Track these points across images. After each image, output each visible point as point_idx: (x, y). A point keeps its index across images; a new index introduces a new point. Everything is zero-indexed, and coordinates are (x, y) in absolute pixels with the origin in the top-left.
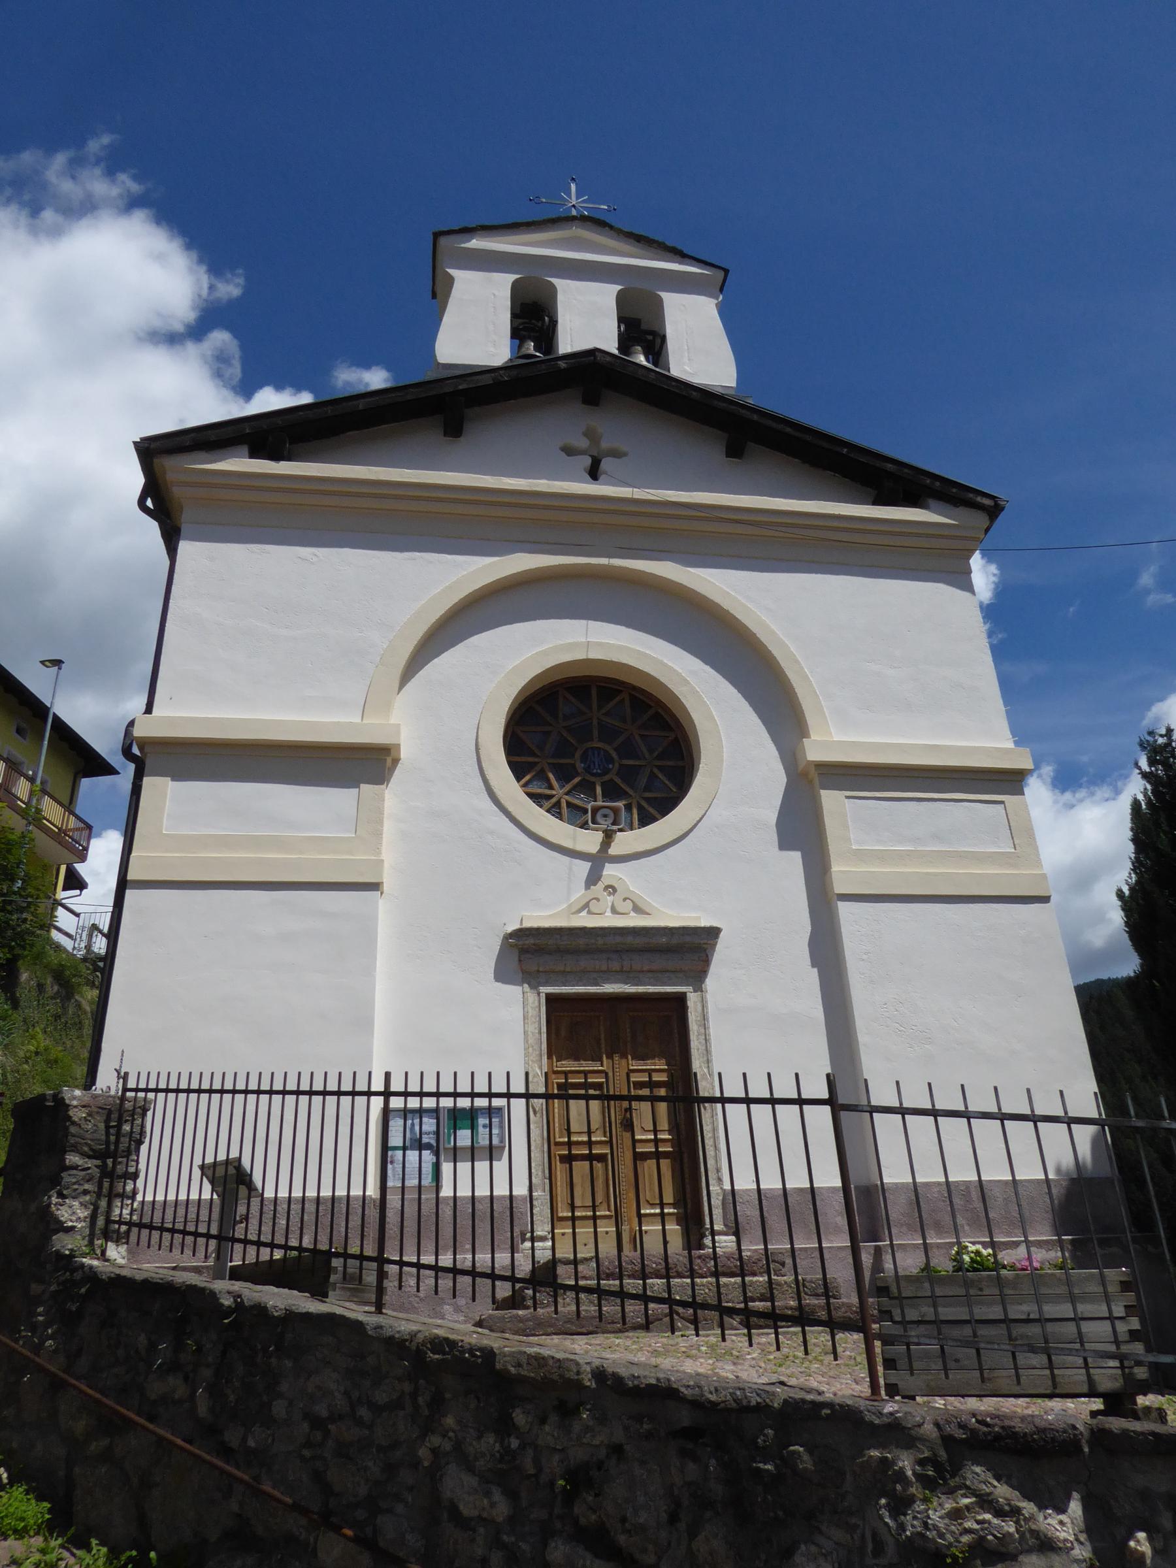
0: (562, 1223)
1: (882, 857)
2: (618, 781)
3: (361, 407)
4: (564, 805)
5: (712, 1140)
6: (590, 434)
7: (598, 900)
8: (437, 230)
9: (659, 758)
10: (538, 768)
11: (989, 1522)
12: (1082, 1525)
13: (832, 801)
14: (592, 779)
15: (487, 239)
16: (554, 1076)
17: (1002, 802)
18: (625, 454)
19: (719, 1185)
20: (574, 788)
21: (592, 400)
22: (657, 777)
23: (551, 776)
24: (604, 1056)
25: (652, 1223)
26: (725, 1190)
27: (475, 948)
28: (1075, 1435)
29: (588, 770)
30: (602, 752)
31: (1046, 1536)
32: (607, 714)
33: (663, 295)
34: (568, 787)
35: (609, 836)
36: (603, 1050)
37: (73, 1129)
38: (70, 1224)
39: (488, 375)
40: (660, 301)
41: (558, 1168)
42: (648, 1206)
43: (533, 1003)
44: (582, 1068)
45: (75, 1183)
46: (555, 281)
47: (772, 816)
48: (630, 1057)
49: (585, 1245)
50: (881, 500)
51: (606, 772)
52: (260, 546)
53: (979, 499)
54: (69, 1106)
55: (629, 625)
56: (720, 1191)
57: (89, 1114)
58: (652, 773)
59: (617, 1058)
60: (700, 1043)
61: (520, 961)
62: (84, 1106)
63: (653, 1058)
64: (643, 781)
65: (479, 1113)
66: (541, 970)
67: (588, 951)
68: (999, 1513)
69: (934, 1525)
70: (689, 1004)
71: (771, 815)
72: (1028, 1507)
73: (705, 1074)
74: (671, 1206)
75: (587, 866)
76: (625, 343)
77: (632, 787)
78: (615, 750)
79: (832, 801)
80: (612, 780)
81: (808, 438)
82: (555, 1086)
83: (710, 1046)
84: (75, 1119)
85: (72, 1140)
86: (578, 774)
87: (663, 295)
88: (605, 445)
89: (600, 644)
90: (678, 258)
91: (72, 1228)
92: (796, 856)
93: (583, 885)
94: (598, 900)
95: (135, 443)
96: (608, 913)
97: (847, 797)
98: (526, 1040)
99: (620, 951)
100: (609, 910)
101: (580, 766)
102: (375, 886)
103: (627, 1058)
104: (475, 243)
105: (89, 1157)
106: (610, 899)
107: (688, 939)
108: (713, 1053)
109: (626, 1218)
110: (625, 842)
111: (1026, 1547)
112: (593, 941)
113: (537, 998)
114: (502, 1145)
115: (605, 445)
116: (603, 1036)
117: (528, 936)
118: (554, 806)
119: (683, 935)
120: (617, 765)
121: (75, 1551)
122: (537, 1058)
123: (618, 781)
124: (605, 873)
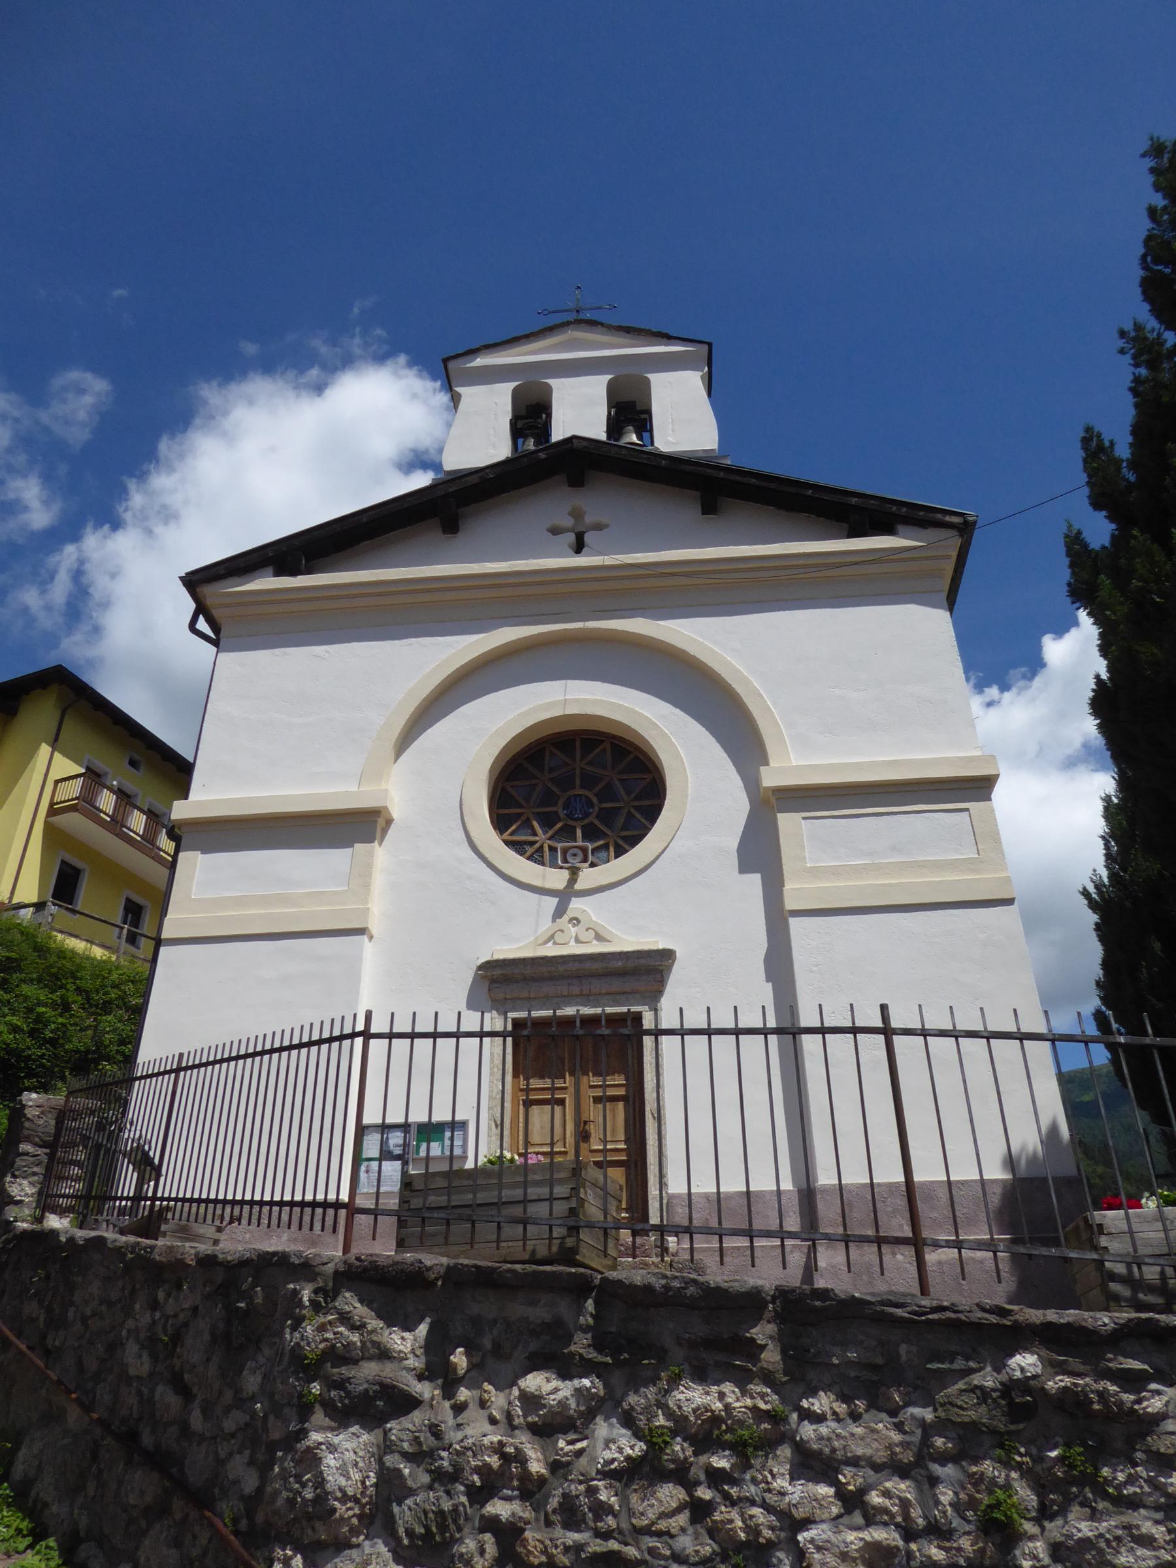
1: (835, 872)
2: (597, 823)
3: (365, 520)
4: (546, 849)
6: (577, 514)
7: (562, 931)
8: (446, 356)
9: (636, 798)
10: (523, 818)
11: (341, 1334)
12: (422, 1343)
13: (788, 822)
14: (573, 823)
15: (499, 354)
17: (967, 810)
18: (607, 526)
20: (556, 833)
21: (577, 482)
22: (634, 816)
23: (535, 824)
24: (567, 1074)
28: (420, 1268)
29: (570, 816)
30: (583, 798)
31: (385, 1347)
32: (590, 763)
33: (649, 376)
34: (550, 833)
35: (574, 872)
37: (27, 1124)
38: (19, 1198)
39: (475, 476)
40: (648, 381)
45: (25, 1166)
46: (550, 381)
47: (734, 843)
48: (591, 1074)
50: (854, 533)
51: (587, 815)
52: (283, 649)
53: (947, 518)
54: (25, 1106)
55: (604, 680)
57: (42, 1113)
58: (629, 813)
61: (489, 990)
62: (38, 1107)
63: (613, 1074)
64: (621, 820)
66: (508, 997)
67: (552, 978)
68: (353, 1328)
69: (307, 1336)
71: (732, 842)
72: (374, 1323)
75: (554, 901)
76: (615, 427)
77: (610, 827)
78: (596, 795)
79: (788, 822)
80: (592, 823)
81: (773, 486)
84: (29, 1116)
85: (26, 1132)
86: (560, 820)
87: (649, 376)
88: (589, 520)
89: (576, 701)
90: (665, 340)
91: (21, 1202)
92: (756, 879)
93: (551, 918)
94: (562, 931)
95: (181, 578)
96: (572, 943)
97: (804, 818)
99: (580, 976)
100: (573, 940)
101: (562, 813)
102: (361, 931)
103: (588, 1075)
104: (480, 361)
105: (40, 1146)
107: (643, 961)
110: (589, 877)
111: (367, 1354)
115: (589, 520)
118: (537, 851)
119: (638, 958)
120: (596, 809)
123: (597, 823)
124: (571, 906)
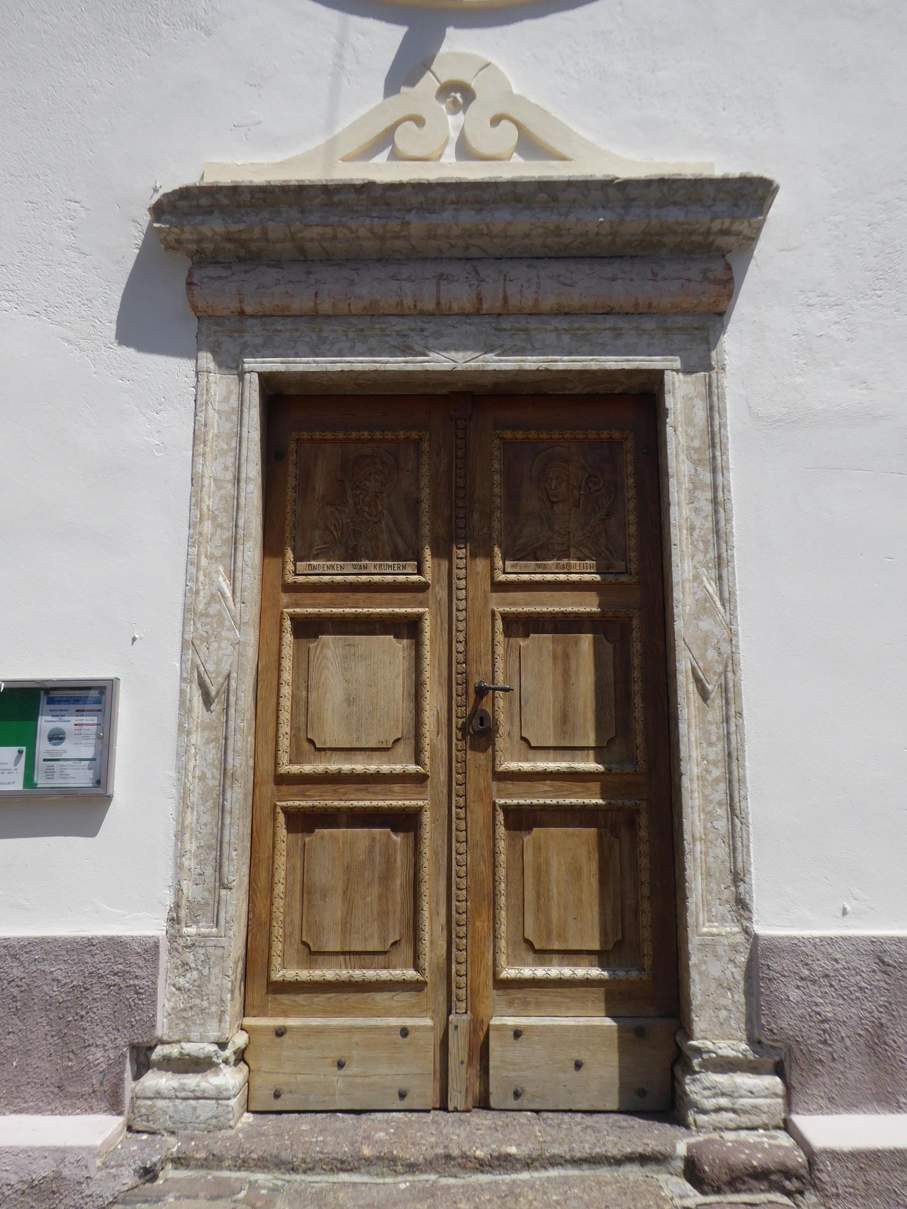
0: (280, 997)
5: (723, 786)
7: (419, 121)
16: (285, 598)
19: (739, 918)
25: (539, 1005)
26: (756, 937)
27: (71, 253)
36: (426, 530)
41: (282, 846)
42: (530, 957)
43: (226, 400)
44: (364, 578)
49: (341, 1065)
56: (740, 938)
59: (462, 553)
60: (697, 510)
61: (190, 284)
65: (43, 699)
70: (670, 401)
73: (708, 598)
74: (595, 958)
82: (288, 624)
83: (728, 521)
94: (419, 121)
98: (196, 501)
100: (450, 151)
103: (490, 555)
106: (454, 123)
107: (673, 215)
108: (736, 540)
109: (462, 992)
112: (394, 225)
113: (235, 388)
114: (99, 791)
116: (425, 493)
117: (208, 211)
121: (491, 715)
122: (225, 549)
124: (445, 48)
